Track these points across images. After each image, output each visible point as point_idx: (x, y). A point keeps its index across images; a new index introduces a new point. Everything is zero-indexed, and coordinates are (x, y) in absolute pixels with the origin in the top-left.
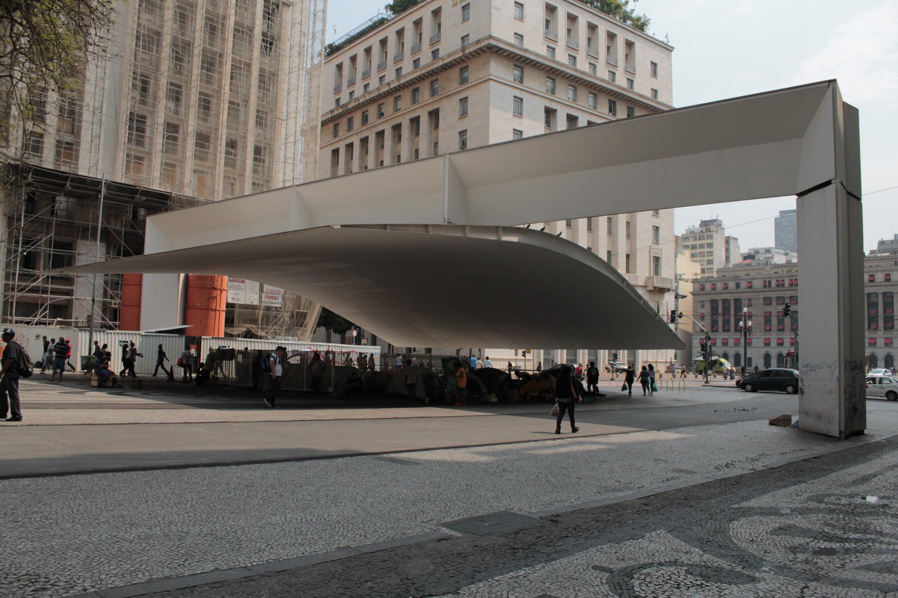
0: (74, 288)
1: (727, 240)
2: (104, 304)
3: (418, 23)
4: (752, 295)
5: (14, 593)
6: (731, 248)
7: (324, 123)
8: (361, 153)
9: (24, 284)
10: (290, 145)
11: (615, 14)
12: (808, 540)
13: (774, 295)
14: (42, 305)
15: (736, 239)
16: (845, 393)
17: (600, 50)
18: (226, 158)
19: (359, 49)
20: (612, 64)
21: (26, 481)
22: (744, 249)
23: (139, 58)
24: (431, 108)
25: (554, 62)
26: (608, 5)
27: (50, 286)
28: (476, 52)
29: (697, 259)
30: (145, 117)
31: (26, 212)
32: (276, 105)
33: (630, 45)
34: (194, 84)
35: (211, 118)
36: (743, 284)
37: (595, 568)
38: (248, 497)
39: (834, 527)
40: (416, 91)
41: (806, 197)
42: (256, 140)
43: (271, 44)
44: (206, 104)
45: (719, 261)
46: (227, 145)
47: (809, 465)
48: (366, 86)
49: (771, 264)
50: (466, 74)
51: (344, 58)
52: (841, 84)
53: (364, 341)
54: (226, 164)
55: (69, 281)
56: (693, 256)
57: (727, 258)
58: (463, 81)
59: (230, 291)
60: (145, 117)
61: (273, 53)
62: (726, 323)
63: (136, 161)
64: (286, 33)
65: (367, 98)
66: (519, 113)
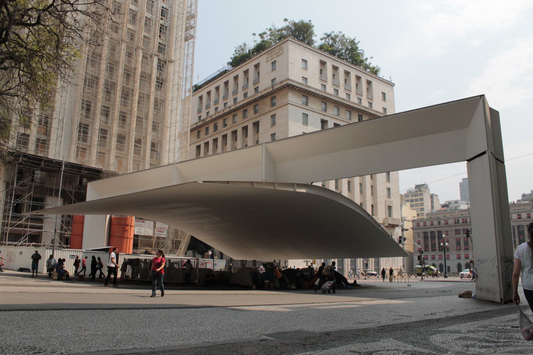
0: (43, 225)
1: (432, 196)
2: (61, 234)
3: (246, 72)
4: (448, 229)
5: (23, 353)
6: (434, 201)
7: (192, 130)
8: (213, 147)
9: (14, 222)
10: (172, 142)
11: (360, 65)
12: (475, 342)
13: (461, 228)
14: (24, 235)
15: (437, 195)
16: (502, 276)
17: (352, 86)
18: (134, 149)
19: (212, 88)
20: (359, 94)
21: (23, 312)
22: (442, 202)
23: (85, 92)
24: (254, 121)
25: (326, 93)
26: (356, 60)
27: (29, 224)
28: (280, 88)
29: (415, 208)
30: (88, 125)
31: (17, 180)
32: (164, 119)
33: (369, 83)
34: (117, 106)
35: (127, 126)
36: (443, 222)
37: (350, 351)
38: (151, 321)
39: (492, 337)
40: (245, 111)
41: (472, 162)
42: (152, 139)
43: (161, 84)
44: (123, 118)
45: (427, 208)
46: (136, 141)
47: (481, 314)
48: (216, 109)
49: (459, 210)
50: (274, 101)
51: (203, 92)
52: (487, 97)
53: (216, 257)
54: (135, 153)
55: (41, 220)
56: (411, 206)
57: (432, 207)
58: (273, 105)
59: (136, 228)
60: (88, 125)
61: (162, 89)
62: (433, 246)
63: (82, 151)
64: (171, 77)
65: (217, 115)
66: (306, 123)
